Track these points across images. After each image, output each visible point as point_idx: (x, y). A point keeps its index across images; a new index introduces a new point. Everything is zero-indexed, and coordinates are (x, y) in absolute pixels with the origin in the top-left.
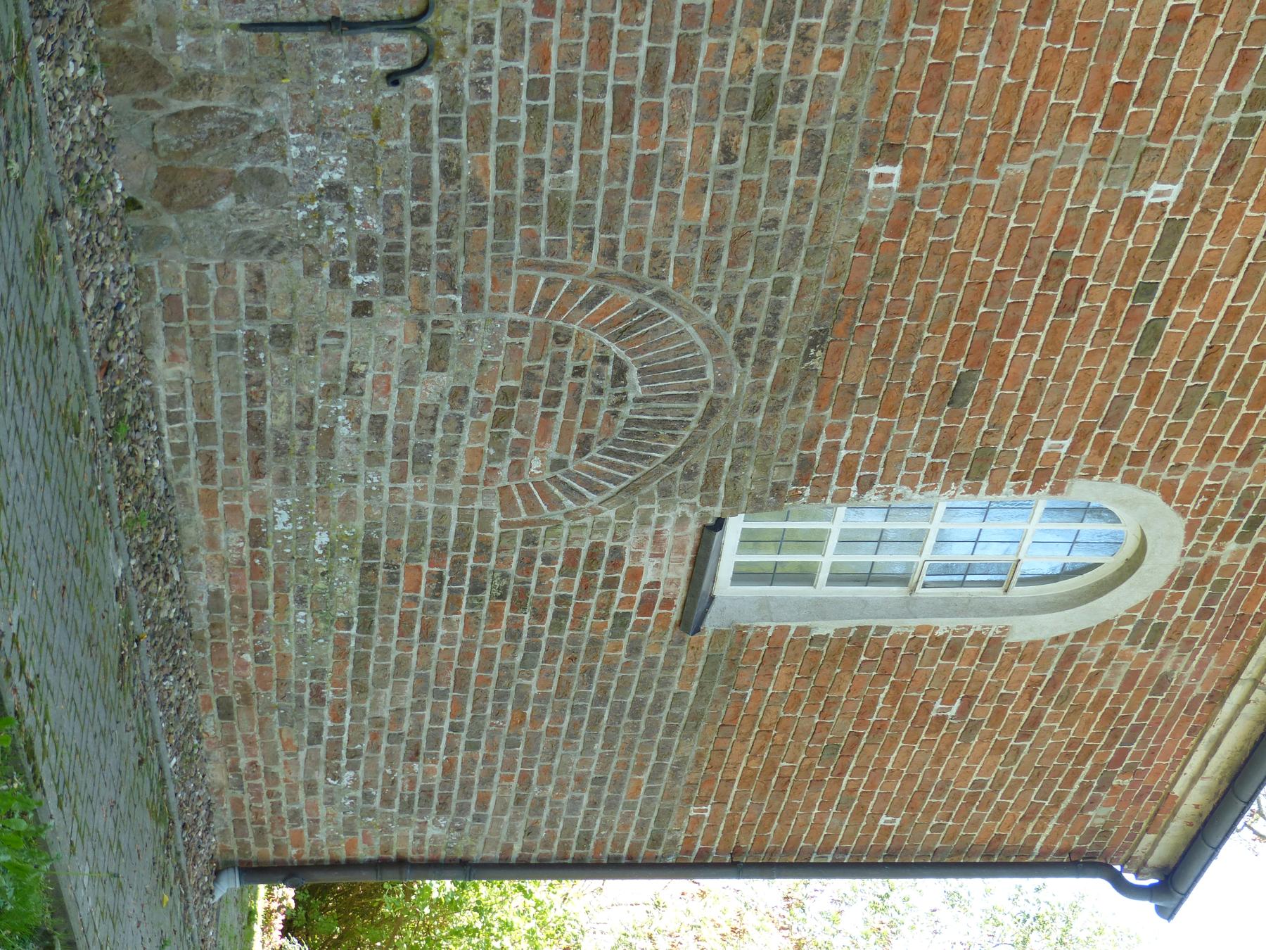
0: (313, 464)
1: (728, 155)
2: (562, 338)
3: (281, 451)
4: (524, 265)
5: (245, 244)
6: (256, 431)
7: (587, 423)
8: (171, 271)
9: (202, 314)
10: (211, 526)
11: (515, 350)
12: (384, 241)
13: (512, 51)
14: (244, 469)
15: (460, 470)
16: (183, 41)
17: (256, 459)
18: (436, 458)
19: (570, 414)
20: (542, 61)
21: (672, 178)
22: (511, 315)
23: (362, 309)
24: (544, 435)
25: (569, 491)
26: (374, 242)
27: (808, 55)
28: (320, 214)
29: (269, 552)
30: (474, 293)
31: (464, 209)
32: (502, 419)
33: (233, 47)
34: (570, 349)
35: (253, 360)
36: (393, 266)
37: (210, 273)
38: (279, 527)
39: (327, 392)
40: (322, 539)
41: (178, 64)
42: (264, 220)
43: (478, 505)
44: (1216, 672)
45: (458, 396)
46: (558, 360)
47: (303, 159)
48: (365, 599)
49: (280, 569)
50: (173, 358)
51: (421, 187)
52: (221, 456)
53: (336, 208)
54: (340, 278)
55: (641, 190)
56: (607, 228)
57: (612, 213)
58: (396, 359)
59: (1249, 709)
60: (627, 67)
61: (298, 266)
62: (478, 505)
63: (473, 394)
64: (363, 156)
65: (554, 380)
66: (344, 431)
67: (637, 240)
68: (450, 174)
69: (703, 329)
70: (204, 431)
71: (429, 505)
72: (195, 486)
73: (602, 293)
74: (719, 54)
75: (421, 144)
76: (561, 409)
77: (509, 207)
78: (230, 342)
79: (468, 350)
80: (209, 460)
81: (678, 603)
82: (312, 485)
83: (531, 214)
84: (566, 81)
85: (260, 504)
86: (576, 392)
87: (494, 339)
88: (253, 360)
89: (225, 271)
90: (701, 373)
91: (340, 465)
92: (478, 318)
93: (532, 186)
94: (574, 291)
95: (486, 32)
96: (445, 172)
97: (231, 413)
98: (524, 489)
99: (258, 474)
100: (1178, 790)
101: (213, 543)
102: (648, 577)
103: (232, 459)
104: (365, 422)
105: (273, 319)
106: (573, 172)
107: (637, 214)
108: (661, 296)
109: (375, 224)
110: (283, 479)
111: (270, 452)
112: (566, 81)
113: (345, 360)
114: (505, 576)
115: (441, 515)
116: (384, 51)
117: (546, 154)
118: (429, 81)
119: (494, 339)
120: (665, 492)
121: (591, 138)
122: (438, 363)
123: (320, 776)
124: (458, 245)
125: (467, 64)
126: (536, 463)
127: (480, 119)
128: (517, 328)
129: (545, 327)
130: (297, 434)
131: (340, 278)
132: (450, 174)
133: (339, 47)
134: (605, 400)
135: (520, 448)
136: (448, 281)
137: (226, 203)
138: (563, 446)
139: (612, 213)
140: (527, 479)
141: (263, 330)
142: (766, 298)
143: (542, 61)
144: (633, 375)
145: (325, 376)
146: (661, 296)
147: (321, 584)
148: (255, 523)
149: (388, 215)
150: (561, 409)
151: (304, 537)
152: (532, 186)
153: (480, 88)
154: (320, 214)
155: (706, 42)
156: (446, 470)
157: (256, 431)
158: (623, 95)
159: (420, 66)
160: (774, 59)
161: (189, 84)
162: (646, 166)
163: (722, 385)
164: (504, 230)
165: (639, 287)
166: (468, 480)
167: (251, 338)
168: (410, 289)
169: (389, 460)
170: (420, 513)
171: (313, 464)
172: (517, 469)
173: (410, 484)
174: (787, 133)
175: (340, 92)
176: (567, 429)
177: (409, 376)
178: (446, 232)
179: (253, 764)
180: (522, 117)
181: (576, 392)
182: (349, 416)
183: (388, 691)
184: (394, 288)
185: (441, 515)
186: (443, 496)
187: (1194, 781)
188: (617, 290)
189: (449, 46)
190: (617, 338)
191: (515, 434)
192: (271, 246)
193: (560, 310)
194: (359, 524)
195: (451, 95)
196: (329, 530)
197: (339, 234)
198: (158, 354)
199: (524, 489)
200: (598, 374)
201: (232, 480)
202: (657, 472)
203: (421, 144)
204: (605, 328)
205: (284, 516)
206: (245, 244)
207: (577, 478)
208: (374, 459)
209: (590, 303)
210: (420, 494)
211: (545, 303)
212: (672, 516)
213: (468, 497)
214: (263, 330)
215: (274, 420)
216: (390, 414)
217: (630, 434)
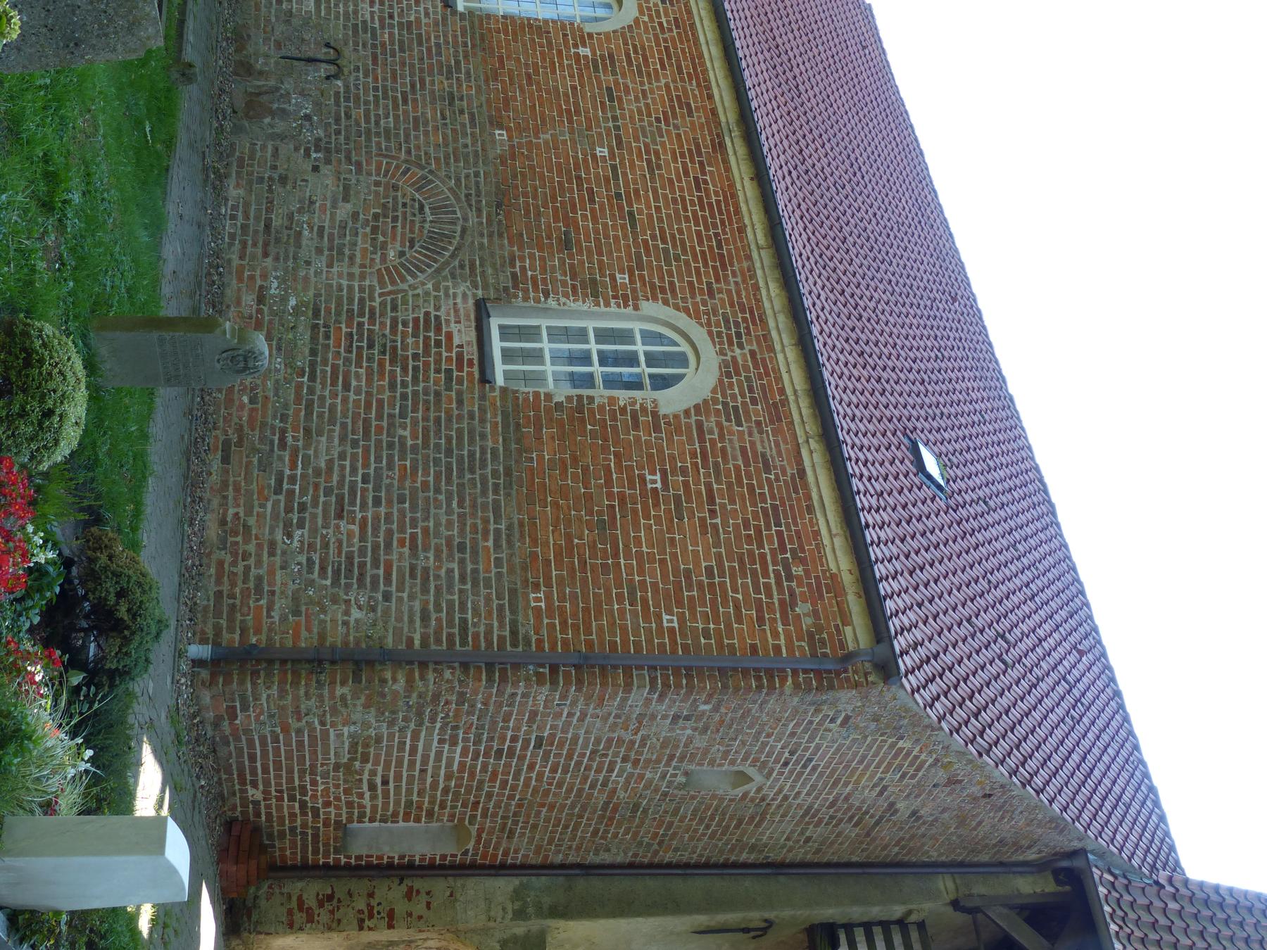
0: (292, 249)
1: (444, 118)
2: (396, 188)
3: (278, 240)
4: (377, 155)
5: (273, 137)
6: (268, 227)
7: (412, 231)
8: (243, 145)
9: (252, 166)
10: (239, 290)
12: (325, 140)
13: (366, 76)
14: (259, 251)
15: (358, 260)
17: (266, 245)
18: (347, 252)
19: (404, 227)
20: (376, 80)
21: (426, 124)
22: (374, 178)
23: (316, 169)
25: (408, 270)
26: (321, 140)
27: (440, 401)
28: (301, 126)
29: (265, 309)
32: (375, 230)
33: (277, 63)
34: (399, 194)
35: (270, 190)
36: (328, 151)
37: (258, 148)
38: (273, 291)
39: (300, 211)
40: (293, 302)
42: (280, 126)
43: (367, 283)
44: (787, 449)
45: (355, 216)
46: (395, 198)
47: (296, 104)
48: (313, 352)
49: (270, 322)
50: (238, 186)
51: (338, 121)
52: (250, 242)
53: (307, 124)
54: (307, 154)
56: (406, 142)
57: (407, 136)
61: (292, 147)
62: (367, 283)
63: (361, 216)
64: (317, 104)
65: (395, 210)
66: (306, 233)
67: (418, 148)
68: (348, 116)
69: (450, 189)
71: (345, 283)
72: (236, 262)
73: (408, 169)
74: (432, 83)
75: (337, 104)
76: (399, 224)
77: (370, 130)
78: (261, 180)
79: (358, 193)
80: (244, 244)
81: (476, 362)
82: (290, 263)
84: (384, 87)
87: (368, 187)
88: (270, 190)
90: (454, 212)
91: (304, 254)
92: (361, 178)
93: (377, 123)
94: (398, 167)
95: (357, 69)
96: (346, 114)
98: (387, 269)
99: (266, 255)
101: (238, 303)
102: (456, 341)
103: (254, 245)
104: (316, 228)
105: (280, 171)
106: (391, 119)
107: (417, 137)
108: (431, 172)
109: (321, 133)
110: (277, 259)
111: (273, 241)
113: (308, 194)
114: (384, 335)
115: (350, 288)
116: (323, 70)
117: (381, 112)
118: (339, 83)
119: (368, 187)
120: (453, 276)
122: (346, 199)
123: (279, 536)
124: (352, 145)
125: (352, 78)
126: (392, 254)
127: (357, 98)
128: (377, 184)
129: (388, 183)
130: (286, 232)
131: (307, 154)
132: (348, 116)
134: (417, 219)
135: (384, 246)
136: (348, 159)
137: (267, 120)
138: (403, 245)
139: (407, 136)
141: (276, 176)
142: (473, 179)
143: (376, 80)
144: (427, 210)
145: (300, 202)
146: (431, 172)
147: (290, 336)
148: (261, 287)
149: (326, 131)
150: (399, 224)
151: (284, 300)
154: (301, 126)
155: (428, 79)
156: (352, 258)
157: (268, 227)
158: (404, 94)
159: (336, 77)
160: (451, 86)
161: (261, 73)
162: (416, 119)
163: (465, 219)
164: (369, 140)
165: (422, 168)
166: (363, 266)
167: (270, 178)
168: (334, 163)
169: (326, 253)
170: (340, 289)
171: (292, 249)
172: (384, 258)
174: (462, 112)
175: (310, 82)
177: (334, 206)
178: (347, 138)
179: (237, 514)
180: (371, 98)
182: (309, 224)
183: (324, 439)
184: (328, 162)
185: (350, 288)
188: (414, 169)
189: (346, 71)
190: (417, 190)
191: (381, 238)
192: (282, 137)
193: (393, 176)
194: (311, 293)
195: (347, 87)
196: (297, 296)
197: (308, 136)
198: (232, 182)
199: (387, 269)
200: (412, 207)
201: (253, 257)
202: (447, 263)
203: (337, 104)
204: (412, 185)
205: (275, 284)
206: (273, 137)
207: (411, 263)
208: (319, 251)
209: (404, 173)
211: (387, 172)
212: (459, 291)
214: (276, 176)
215: (277, 222)
216: (326, 225)
217: (431, 238)
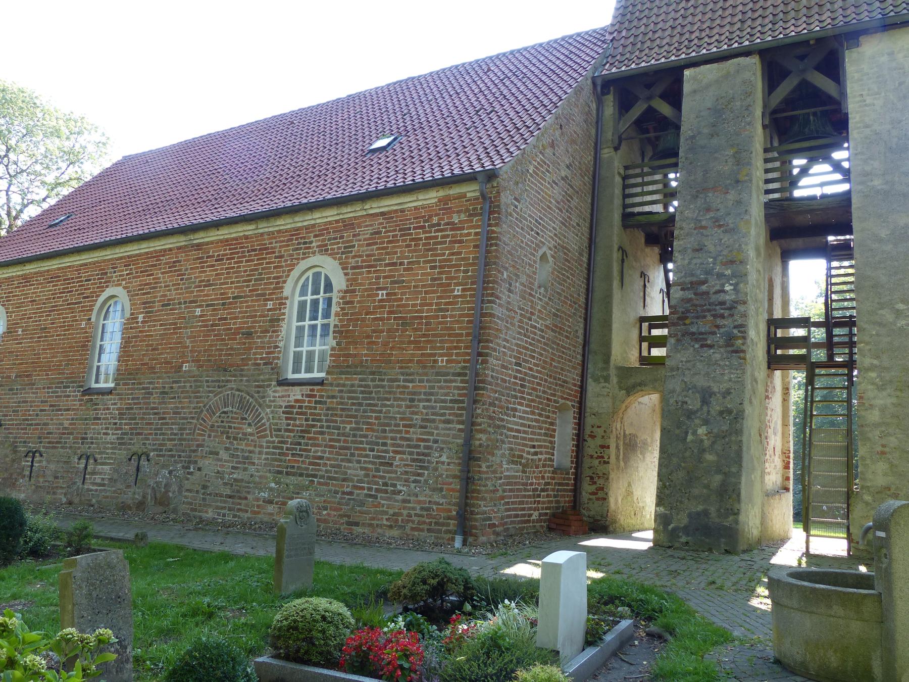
2: (212, 426)
3: (238, 491)
5: (180, 491)
6: (230, 497)
7: (237, 418)
10: (264, 513)
11: (215, 436)
13: (148, 439)
15: (252, 448)
16: (137, 496)
17: (240, 498)
18: (247, 454)
20: (151, 434)
21: (177, 408)
23: (199, 469)
24: (240, 428)
25: (259, 422)
28: (175, 476)
30: (198, 446)
31: (178, 447)
32: (235, 439)
33: (139, 488)
35: (210, 494)
36: (190, 462)
39: (222, 478)
40: (273, 485)
41: (140, 498)
42: (175, 487)
45: (227, 449)
46: (218, 427)
51: (173, 456)
54: (191, 473)
55: (179, 413)
58: (214, 463)
59: (232, 231)
60: (154, 419)
65: (225, 427)
66: (235, 476)
68: (171, 450)
69: (215, 396)
70: (230, 509)
71: (264, 456)
72: (249, 515)
74: (154, 403)
75: (163, 456)
78: (204, 499)
79: (214, 447)
80: (239, 510)
83: (182, 434)
85: (258, 500)
86: (227, 422)
88: (210, 494)
89: (186, 497)
91: (246, 478)
93: (175, 434)
94: (201, 425)
97: (225, 502)
99: (246, 498)
100: (434, 201)
101: (272, 514)
103: (240, 504)
107: (185, 413)
108: (204, 406)
110: (249, 493)
112: (155, 429)
115: (267, 453)
116: (143, 462)
118: (152, 454)
120: (264, 397)
121: (167, 424)
122: (217, 454)
127: (160, 445)
128: (209, 436)
131: (191, 473)
132: (171, 450)
133: (142, 469)
134: (230, 415)
135: (245, 434)
136: (194, 451)
137: (171, 494)
138: (245, 424)
140: (255, 432)
142: (210, 384)
143: (151, 434)
146: (204, 406)
151: (271, 489)
152: (175, 434)
153: (154, 445)
154: (175, 476)
155: (152, 405)
156: (250, 452)
157: (230, 497)
158: (160, 419)
159: (148, 456)
160: (157, 393)
161: (144, 497)
163: (232, 389)
164: (184, 440)
165: (202, 411)
166: (255, 446)
170: (267, 459)
173: (256, 461)
174: (172, 388)
176: (239, 423)
177: (221, 460)
181: (227, 422)
184: (196, 462)
185: (267, 453)
186: (260, 453)
187: (327, 217)
190: (214, 414)
192: (180, 487)
193: (206, 427)
195: (154, 450)
196: (270, 482)
201: (247, 505)
202: (256, 400)
203: (163, 456)
205: (263, 494)
206: (180, 491)
209: (204, 421)
210: (259, 459)
211: (203, 430)
213: (261, 446)
